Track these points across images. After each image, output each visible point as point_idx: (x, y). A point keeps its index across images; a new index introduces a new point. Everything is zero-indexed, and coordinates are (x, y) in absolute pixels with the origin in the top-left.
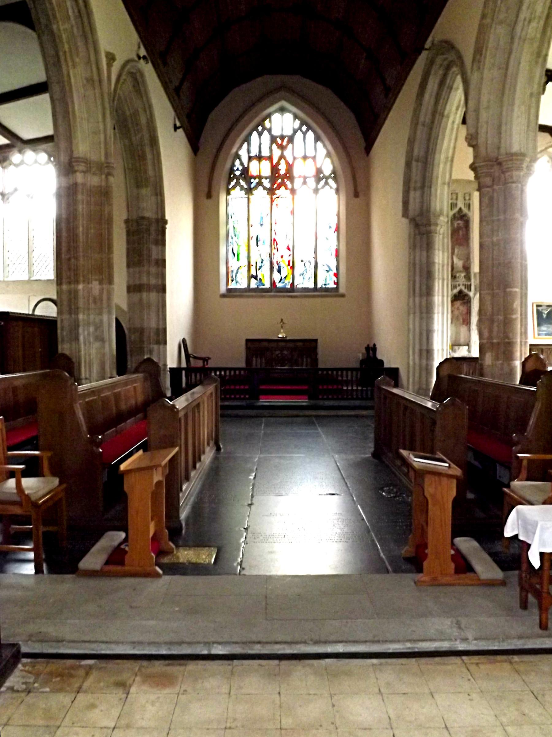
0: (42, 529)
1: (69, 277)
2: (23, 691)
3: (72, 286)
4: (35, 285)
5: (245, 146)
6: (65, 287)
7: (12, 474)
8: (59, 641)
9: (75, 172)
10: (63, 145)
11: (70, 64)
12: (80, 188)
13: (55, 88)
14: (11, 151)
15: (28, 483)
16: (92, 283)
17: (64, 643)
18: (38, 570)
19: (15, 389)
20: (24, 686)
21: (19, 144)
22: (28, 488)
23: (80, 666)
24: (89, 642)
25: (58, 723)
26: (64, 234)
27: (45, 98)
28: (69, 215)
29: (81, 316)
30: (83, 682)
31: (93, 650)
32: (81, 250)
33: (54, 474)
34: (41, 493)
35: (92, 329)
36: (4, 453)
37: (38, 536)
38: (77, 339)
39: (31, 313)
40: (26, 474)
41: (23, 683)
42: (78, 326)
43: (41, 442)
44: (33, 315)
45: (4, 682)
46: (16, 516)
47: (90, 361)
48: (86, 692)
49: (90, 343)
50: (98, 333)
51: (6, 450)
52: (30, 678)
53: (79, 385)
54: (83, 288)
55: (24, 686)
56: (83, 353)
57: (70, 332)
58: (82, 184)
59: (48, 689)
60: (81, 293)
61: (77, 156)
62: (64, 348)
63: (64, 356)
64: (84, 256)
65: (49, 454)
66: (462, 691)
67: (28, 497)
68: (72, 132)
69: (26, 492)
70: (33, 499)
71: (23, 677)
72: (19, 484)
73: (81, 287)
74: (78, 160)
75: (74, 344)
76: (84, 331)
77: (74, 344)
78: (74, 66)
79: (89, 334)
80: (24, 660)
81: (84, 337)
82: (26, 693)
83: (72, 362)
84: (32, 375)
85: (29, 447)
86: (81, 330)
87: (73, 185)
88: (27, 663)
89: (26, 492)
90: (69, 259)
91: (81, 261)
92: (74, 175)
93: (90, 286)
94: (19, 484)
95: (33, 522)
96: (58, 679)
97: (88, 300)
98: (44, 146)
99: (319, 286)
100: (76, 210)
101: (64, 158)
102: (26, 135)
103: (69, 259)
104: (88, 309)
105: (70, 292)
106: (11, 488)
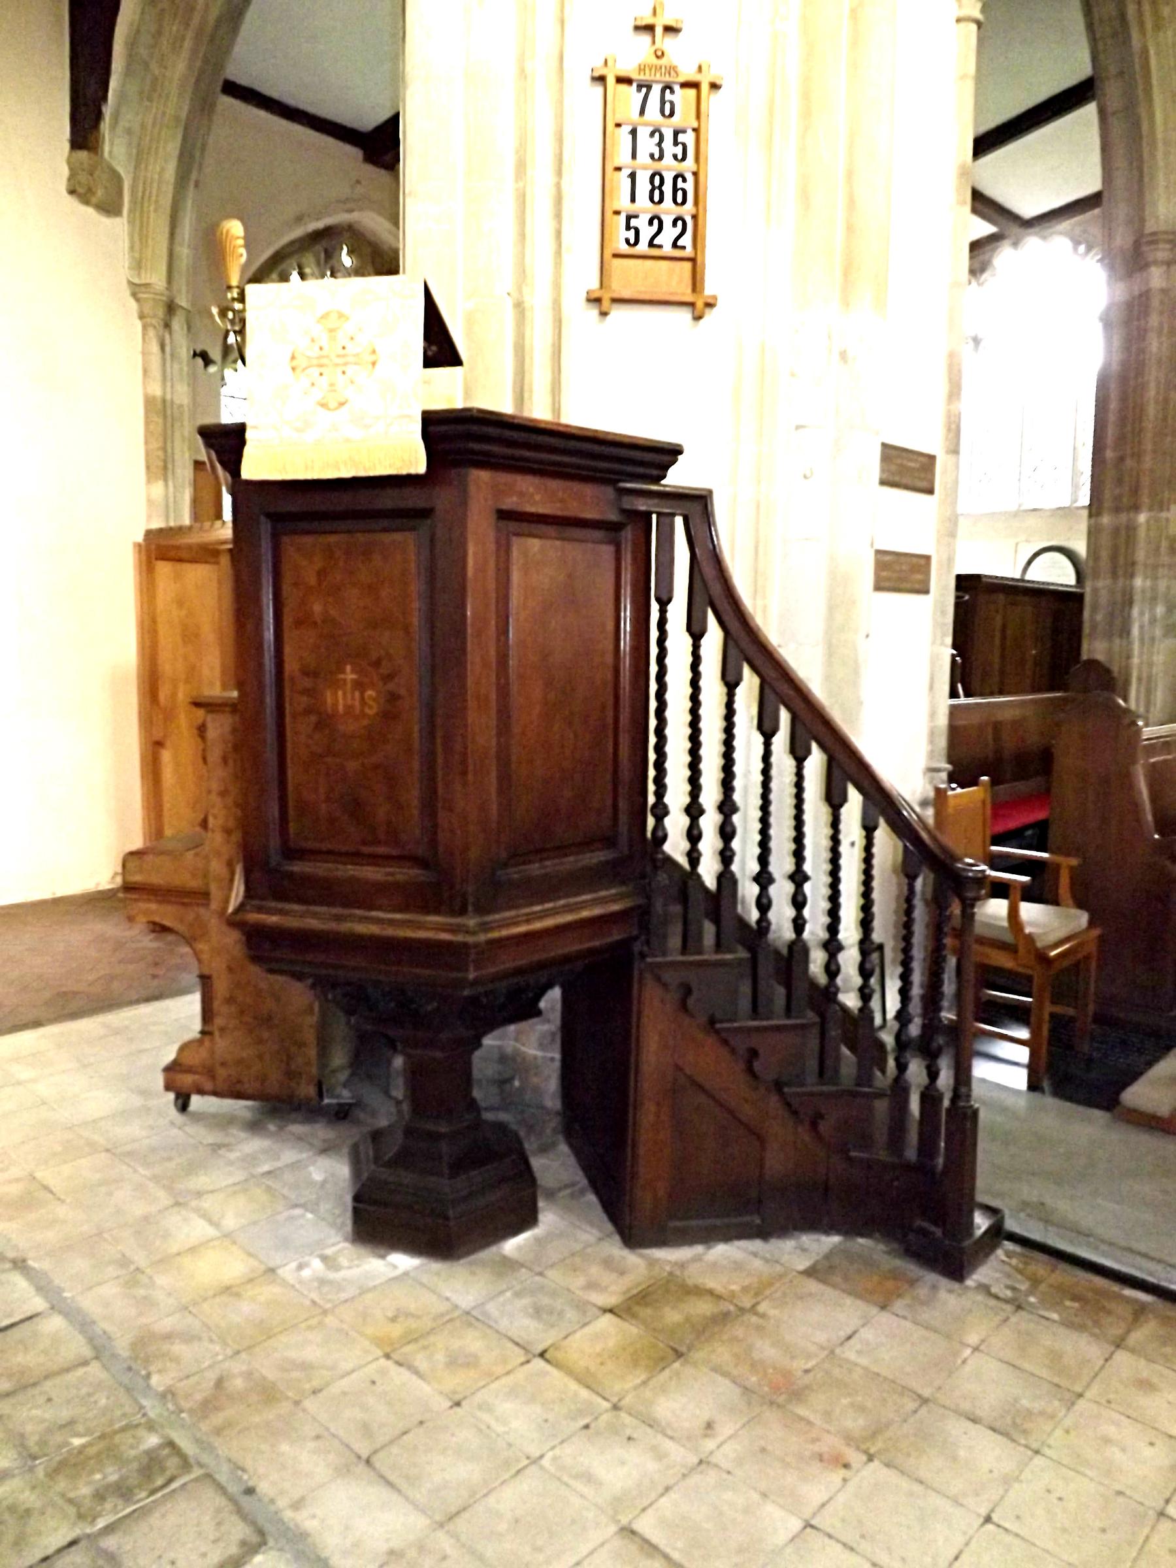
0: (1049, 1008)
1: (1118, 498)
2: (1006, 1301)
3: (1123, 518)
4: (1032, 521)
6: (1106, 520)
7: (1000, 890)
8: (1084, 1234)
9: (1146, 266)
10: (1121, 211)
11: (1149, 25)
12: (1155, 302)
13: (1112, 90)
14: (997, 248)
15: (1030, 911)
16: (1168, 510)
17: (1091, 1239)
18: (1033, 1086)
19: (997, 727)
21: (1015, 230)
22: (1031, 924)
24: (1145, 1256)
25: (1078, 1388)
26: (1113, 405)
27: (1089, 111)
28: (1125, 364)
29: (1138, 582)
30: (1128, 1331)
31: (1151, 1274)
32: (1149, 435)
33: (1080, 904)
34: (1053, 938)
35: (1160, 610)
36: (985, 847)
37: (1040, 1021)
38: (1125, 631)
39: (1018, 576)
40: (1031, 895)
42: (1131, 603)
43: (1054, 834)
44: (1022, 580)
46: (999, 970)
47: (1150, 677)
49: (1153, 639)
51: (988, 841)
53: (1147, 725)
54: (1148, 522)
55: (1009, 1293)
56: (1136, 661)
57: (1112, 615)
58: (1163, 291)
59: (1055, 1316)
60: (1142, 533)
61: (1154, 229)
62: (1094, 648)
63: (1093, 664)
64: (1154, 452)
65: (1074, 862)
67: (1030, 939)
68: (1146, 179)
69: (1027, 930)
70: (1039, 944)
71: (1009, 1276)
72: (1013, 913)
73: (1142, 518)
74: (1154, 239)
75: (1117, 641)
76: (1142, 614)
77: (1117, 641)
78: (1158, 27)
79: (1153, 621)
80: (1009, 1245)
81: (1141, 627)
83: (1113, 679)
84: (1031, 700)
85: (1014, 842)
86: (1135, 611)
87: (1141, 295)
88: (1014, 1252)
89: (1027, 930)
90: (1121, 459)
91: (1148, 462)
92: (1145, 274)
93: (1164, 515)
94: (1013, 913)
95: (1035, 990)
96: (1076, 1305)
97: (1158, 549)
98: (1066, 225)
100: (1142, 351)
101: (1123, 238)
102: (1028, 209)
103: (1121, 459)
104: (1155, 567)
105: (1116, 531)
106: (995, 918)
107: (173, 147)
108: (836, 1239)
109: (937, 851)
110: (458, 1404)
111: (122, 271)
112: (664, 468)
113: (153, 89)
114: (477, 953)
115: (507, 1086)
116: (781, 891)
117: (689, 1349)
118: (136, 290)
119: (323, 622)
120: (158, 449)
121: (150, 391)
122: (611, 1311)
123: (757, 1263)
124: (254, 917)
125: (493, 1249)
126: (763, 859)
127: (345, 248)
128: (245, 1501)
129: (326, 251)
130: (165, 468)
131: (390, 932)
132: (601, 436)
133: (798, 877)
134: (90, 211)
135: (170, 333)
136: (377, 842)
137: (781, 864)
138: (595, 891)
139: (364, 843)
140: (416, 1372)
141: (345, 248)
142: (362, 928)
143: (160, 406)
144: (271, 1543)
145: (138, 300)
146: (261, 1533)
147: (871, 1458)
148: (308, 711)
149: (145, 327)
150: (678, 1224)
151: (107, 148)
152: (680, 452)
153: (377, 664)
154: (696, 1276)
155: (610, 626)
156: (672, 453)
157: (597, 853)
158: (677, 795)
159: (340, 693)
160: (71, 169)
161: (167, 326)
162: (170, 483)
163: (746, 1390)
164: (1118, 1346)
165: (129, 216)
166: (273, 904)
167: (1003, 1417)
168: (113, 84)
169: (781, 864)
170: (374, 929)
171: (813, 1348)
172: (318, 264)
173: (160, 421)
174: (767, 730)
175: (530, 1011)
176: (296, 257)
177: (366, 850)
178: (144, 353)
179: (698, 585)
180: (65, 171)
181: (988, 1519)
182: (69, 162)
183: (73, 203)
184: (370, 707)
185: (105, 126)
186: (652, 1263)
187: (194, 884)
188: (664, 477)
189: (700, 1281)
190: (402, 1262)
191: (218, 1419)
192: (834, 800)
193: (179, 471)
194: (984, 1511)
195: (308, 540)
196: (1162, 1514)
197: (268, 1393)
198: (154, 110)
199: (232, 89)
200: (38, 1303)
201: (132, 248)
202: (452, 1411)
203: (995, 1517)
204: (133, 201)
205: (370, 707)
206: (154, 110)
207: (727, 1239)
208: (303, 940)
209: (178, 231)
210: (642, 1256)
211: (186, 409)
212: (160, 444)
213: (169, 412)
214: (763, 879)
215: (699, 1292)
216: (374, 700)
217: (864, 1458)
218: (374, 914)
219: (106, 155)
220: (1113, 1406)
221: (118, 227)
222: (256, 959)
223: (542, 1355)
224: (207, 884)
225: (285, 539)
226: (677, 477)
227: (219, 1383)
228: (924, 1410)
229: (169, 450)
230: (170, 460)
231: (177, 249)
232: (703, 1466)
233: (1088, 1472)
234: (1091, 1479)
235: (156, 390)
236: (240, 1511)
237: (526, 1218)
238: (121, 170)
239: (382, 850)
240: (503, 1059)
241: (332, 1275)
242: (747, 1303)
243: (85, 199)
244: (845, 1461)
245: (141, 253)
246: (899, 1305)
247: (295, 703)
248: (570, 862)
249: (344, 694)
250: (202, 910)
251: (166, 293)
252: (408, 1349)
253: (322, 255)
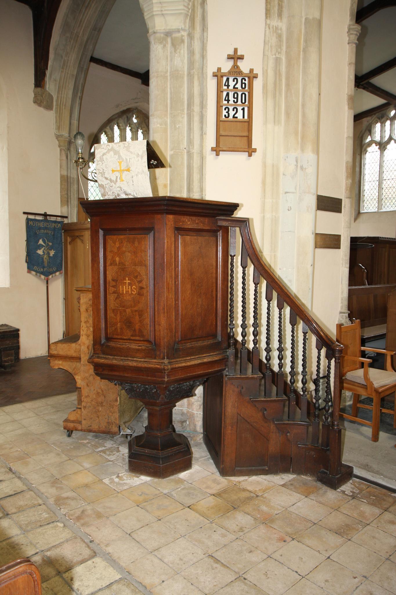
2: (350, 496)
5: (137, 126)
14: (387, 109)
15: (373, 372)
20: (351, 494)
23: (390, 495)
40: (371, 365)
41: (351, 492)
45: (340, 486)
48: (390, 512)
50: (244, 276)
52: (356, 490)
55: (351, 494)
59: (365, 501)
66: (80, 428)
71: (353, 489)
72: (366, 374)
82: (352, 498)
94: (366, 374)
96: (374, 498)
99: (122, 169)
107: (71, 86)
108: (295, 476)
109: (327, 340)
110: (160, 520)
111: (52, 130)
112: (232, 212)
113: (64, 65)
114: (168, 372)
115: (184, 424)
116: (275, 354)
117: (238, 507)
118: (58, 137)
119: (119, 263)
120: (65, 194)
121: (62, 173)
122: (213, 495)
123: (266, 482)
124: (97, 360)
125: (176, 476)
126: (268, 343)
127: (135, 116)
128: (91, 545)
129: (127, 117)
130: (68, 201)
131: (140, 365)
132: (210, 203)
133: (281, 350)
134: (41, 109)
135: (70, 152)
136: (135, 336)
137: (275, 344)
138: (209, 353)
139: (132, 336)
140: (147, 511)
141: (135, 116)
142: (131, 364)
143: (66, 179)
144: (98, 555)
145: (58, 140)
146: (95, 552)
147: (293, 539)
148: (114, 292)
149: (61, 150)
150: (239, 468)
151: (47, 87)
152: (238, 206)
153: (136, 277)
154: (244, 485)
155: (214, 264)
156: (234, 207)
157: (210, 341)
158: (239, 321)
159: (124, 287)
160: (35, 95)
161: (69, 149)
162: (69, 207)
163: (255, 519)
164: (386, 511)
165: (55, 110)
166: (102, 356)
167: (340, 529)
168: (50, 63)
169: (275, 344)
170: (135, 364)
171: (280, 508)
172: (125, 123)
173: (66, 184)
174: (269, 299)
175: (189, 393)
176: (116, 120)
177: (132, 338)
178: (61, 160)
179: (244, 251)
180: (33, 95)
181: (329, 558)
182: (34, 92)
183: (35, 107)
184: (134, 291)
185: (47, 79)
186: (230, 481)
187: (74, 355)
188: (233, 214)
189: (245, 487)
190: (145, 478)
191: (82, 521)
192: (293, 323)
193: (72, 202)
194: (328, 556)
195: (115, 237)
196: (387, 559)
197: (99, 516)
198: (64, 72)
199: (93, 60)
200: (25, 488)
201: (56, 122)
202: (157, 522)
203: (331, 557)
204: (57, 105)
205: (134, 291)
206: (64, 72)
207: (256, 474)
208: (112, 368)
209: (73, 115)
210: (226, 479)
211: (75, 179)
212: (66, 192)
213: (69, 180)
214: (268, 350)
215: (244, 490)
216: (135, 289)
217: (291, 539)
218: (135, 359)
219: (47, 89)
220: (379, 528)
221: (50, 115)
222: (97, 374)
223: (188, 507)
224: (80, 355)
225: (107, 237)
226: (239, 214)
227: (83, 512)
228: (315, 526)
229: (69, 195)
230: (69, 198)
231: (72, 121)
232: (237, 540)
233: (366, 547)
234: (366, 548)
235: (65, 173)
236: (88, 547)
237: (187, 465)
238: (52, 94)
239: (137, 338)
240: (183, 414)
241: (121, 482)
242: (260, 494)
243: (40, 105)
244: (284, 540)
245: (60, 123)
246: (312, 496)
247: (111, 290)
248: (200, 344)
249: (126, 287)
250: (78, 364)
251: (69, 138)
252: (145, 504)
253: (126, 119)
